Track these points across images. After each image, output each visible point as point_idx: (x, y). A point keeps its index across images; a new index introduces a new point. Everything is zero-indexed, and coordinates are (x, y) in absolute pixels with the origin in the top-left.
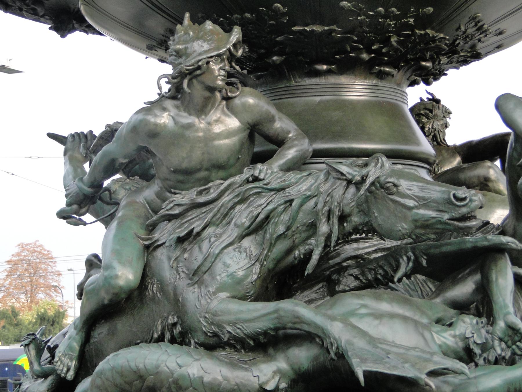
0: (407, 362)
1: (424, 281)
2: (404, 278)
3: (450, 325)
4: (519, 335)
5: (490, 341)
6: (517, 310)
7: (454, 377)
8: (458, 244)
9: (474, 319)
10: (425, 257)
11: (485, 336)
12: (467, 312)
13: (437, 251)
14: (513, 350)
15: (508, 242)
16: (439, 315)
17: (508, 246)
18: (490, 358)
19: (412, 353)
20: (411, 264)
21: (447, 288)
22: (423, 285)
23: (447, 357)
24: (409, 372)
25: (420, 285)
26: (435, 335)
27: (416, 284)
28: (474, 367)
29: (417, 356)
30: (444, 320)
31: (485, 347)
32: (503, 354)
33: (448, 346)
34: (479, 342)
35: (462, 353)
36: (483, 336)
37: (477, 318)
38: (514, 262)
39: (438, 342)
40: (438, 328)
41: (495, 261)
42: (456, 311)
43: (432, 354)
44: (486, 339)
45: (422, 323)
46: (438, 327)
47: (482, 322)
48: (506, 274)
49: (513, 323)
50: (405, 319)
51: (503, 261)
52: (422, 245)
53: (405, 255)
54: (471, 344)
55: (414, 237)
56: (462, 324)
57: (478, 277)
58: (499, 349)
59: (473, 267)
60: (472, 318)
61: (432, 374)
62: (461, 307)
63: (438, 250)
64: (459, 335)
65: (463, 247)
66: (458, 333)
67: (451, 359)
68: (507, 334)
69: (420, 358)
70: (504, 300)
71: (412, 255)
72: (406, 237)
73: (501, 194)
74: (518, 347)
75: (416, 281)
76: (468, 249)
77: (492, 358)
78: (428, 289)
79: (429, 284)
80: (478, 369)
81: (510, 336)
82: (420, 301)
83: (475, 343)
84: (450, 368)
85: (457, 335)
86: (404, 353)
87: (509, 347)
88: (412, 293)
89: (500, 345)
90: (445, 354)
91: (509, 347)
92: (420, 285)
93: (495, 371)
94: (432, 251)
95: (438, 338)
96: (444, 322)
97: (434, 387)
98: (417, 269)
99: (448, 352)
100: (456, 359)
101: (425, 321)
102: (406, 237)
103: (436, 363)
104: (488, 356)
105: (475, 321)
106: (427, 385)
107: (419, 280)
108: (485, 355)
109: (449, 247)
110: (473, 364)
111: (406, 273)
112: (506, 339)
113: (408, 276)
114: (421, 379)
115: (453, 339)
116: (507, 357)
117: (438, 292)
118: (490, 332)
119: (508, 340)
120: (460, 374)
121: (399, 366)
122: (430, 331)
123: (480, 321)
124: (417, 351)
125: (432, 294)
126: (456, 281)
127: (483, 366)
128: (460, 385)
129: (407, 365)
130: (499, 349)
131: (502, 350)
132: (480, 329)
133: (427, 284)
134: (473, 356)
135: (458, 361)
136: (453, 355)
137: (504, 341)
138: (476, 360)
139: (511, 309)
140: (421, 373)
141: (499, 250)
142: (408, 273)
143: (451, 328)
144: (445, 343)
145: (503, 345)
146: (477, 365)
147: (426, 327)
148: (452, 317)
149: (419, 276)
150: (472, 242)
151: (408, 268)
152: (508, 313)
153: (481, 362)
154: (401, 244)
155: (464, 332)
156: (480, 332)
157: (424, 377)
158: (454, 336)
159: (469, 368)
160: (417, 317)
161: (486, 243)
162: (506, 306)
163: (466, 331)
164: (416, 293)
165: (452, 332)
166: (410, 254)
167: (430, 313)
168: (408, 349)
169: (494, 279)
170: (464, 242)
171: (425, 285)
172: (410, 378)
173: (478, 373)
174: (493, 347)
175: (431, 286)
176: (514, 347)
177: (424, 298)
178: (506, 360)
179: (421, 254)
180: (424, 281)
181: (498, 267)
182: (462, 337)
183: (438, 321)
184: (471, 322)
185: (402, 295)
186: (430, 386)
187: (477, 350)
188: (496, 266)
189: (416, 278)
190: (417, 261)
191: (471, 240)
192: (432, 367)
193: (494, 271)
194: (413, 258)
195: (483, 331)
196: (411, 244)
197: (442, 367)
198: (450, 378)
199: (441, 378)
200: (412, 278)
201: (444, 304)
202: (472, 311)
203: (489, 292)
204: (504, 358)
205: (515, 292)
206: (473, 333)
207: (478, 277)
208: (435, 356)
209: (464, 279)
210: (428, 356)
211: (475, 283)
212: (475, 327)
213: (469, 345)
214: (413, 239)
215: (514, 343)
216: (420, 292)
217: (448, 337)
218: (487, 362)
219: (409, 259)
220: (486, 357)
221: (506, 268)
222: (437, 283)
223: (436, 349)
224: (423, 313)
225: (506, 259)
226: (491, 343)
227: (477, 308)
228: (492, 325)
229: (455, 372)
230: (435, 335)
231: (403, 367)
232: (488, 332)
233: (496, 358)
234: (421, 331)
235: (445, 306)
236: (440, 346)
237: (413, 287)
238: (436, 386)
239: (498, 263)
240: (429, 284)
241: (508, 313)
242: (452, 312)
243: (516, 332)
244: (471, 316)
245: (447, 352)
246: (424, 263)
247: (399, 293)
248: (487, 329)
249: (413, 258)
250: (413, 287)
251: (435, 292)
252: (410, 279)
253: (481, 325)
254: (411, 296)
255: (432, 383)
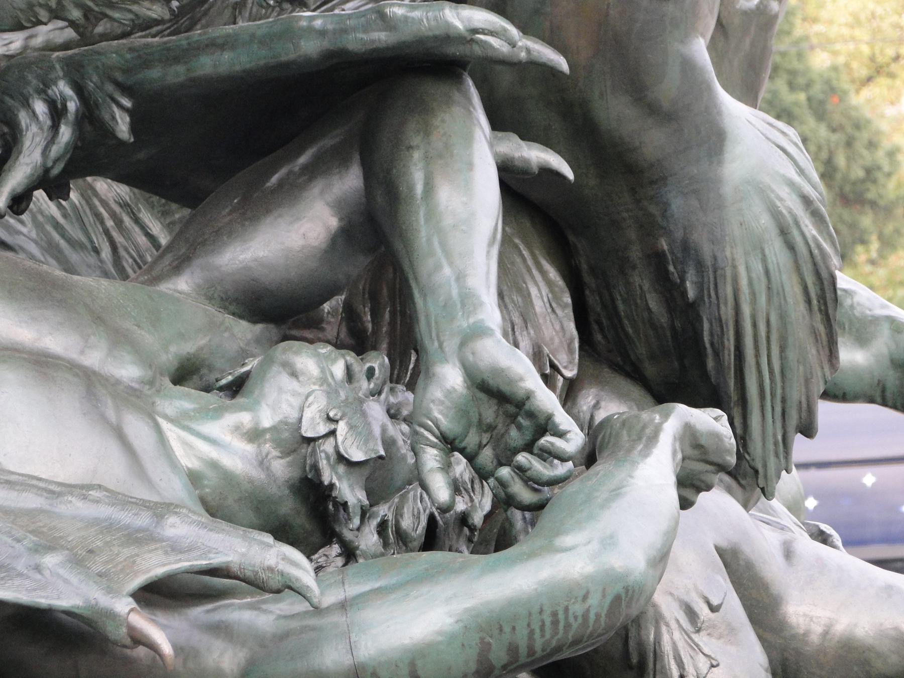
0: (50, 547)
1: (124, 205)
2: (40, 195)
3: (236, 388)
4: (523, 421)
5: (404, 449)
6: (517, 319)
7: (252, 607)
8: (266, 41)
9: (334, 361)
10: (127, 103)
11: (384, 430)
12: (308, 334)
13: (176, 74)
14: (502, 483)
15: (475, 31)
16: (189, 348)
17: (477, 50)
18: (406, 523)
19: (76, 507)
20: (66, 133)
21: (218, 232)
22: (119, 223)
23: (223, 525)
24: (59, 588)
25: (110, 223)
26: (172, 432)
27: (89, 218)
28: (340, 561)
29: (96, 522)
30: (211, 368)
31: (383, 476)
32: (461, 506)
33: (228, 477)
34: (357, 456)
35: (288, 507)
36: (377, 431)
37: (351, 357)
38: (499, 121)
39: (188, 462)
40: (180, 401)
41: (423, 109)
42: (259, 327)
43: (162, 509)
44: (389, 443)
45: (118, 382)
46: (183, 400)
47: (370, 373)
48: (470, 166)
49: (498, 372)
50: (41, 364)
51: (457, 110)
52: (113, 52)
53: (42, 92)
54: (323, 464)
55: (76, 14)
56: (285, 380)
57: (350, 181)
58: (440, 481)
59: (327, 142)
60: (327, 357)
61: (159, 594)
62: (282, 311)
63: (181, 69)
64: (274, 429)
65: (288, 53)
66: (267, 420)
67: (241, 530)
68: (475, 420)
69: (107, 527)
70: (460, 277)
71: (68, 91)
72: (43, 15)
73: (677, 523)
74: (521, 470)
75: (92, 207)
76: (308, 61)
77: (413, 523)
78: (142, 240)
79: (146, 217)
80: (352, 568)
81: (491, 428)
82: (106, 289)
83: (341, 458)
84: (235, 569)
85: (265, 431)
86: (41, 511)
87: (483, 475)
88: (74, 257)
89: (447, 467)
90: (215, 510)
91: (483, 475)
92: (110, 223)
93: (427, 577)
94: (155, 73)
95: (185, 443)
96: (212, 377)
97: (167, 648)
98: (91, 154)
99: (230, 501)
100: (263, 528)
101: (128, 371)
102: (43, 15)
103: (175, 548)
104: (398, 514)
105: (338, 370)
106: (138, 639)
107: (105, 203)
108: (384, 510)
109: (227, 56)
110: (335, 549)
111: (47, 171)
112: (471, 440)
113: (54, 184)
114: (111, 615)
115: (249, 448)
116: (477, 519)
117: (182, 253)
118: (405, 412)
119: (481, 446)
120: (278, 591)
121: (20, 565)
122: (151, 415)
123: (360, 369)
124: (97, 501)
125: (161, 257)
126: (256, 205)
127: (375, 556)
128: (282, 637)
129: (51, 560)
130: (440, 481)
131: (456, 488)
132: (361, 402)
133: (137, 221)
134: (336, 520)
135: (269, 539)
136: (251, 516)
137: (462, 451)
138: (348, 535)
139: (491, 314)
140: (110, 591)
141: (433, 65)
142: (56, 171)
143: (240, 400)
144: (214, 465)
145: (461, 467)
146: (350, 554)
147: (133, 398)
148: (243, 355)
149: (103, 186)
150: (322, 33)
151: (55, 151)
152: (479, 331)
153: (369, 540)
154: (25, 48)
155: (293, 415)
156: (364, 414)
157: (123, 605)
158: (255, 435)
159: (318, 569)
160: (94, 358)
161: (381, 37)
162: (468, 300)
163: (302, 410)
164: (92, 259)
165: (245, 418)
166: (63, 88)
167: (148, 338)
168: (57, 491)
169: (419, 189)
170: (289, 33)
171: (127, 221)
172: (68, 613)
173: (353, 589)
174: (418, 479)
175: (156, 228)
176: (505, 472)
177: (124, 276)
178: (472, 529)
179: (110, 88)
180: (124, 205)
181: (435, 137)
182: (286, 435)
183: (185, 374)
184: (323, 371)
185: (29, 263)
186: (152, 647)
187: (351, 493)
188: (427, 134)
189: (89, 194)
190: (90, 119)
191: (318, 23)
192: (156, 566)
193: (417, 155)
194: (72, 106)
195: (376, 411)
196: (66, 46)
197: (203, 563)
198: (239, 612)
199: (199, 612)
200: (74, 196)
201: (210, 298)
202: (331, 331)
203: (399, 246)
204: (464, 519)
205: (506, 241)
206: (330, 419)
207: (350, 181)
208: (172, 520)
209: (290, 192)
210: (143, 520)
211: (338, 206)
212: (343, 395)
213: (316, 468)
214: (73, 24)
215: (505, 458)
216: (106, 253)
217: (227, 438)
218: (394, 537)
219: (57, 112)
220: (390, 517)
221: (468, 139)
222: (181, 213)
223: (175, 488)
224: (120, 339)
225: (469, 113)
226: (411, 460)
227: (350, 314)
228: (411, 386)
229: (258, 585)
230: (172, 432)
231: (38, 568)
232: (393, 414)
233: (432, 519)
234: (111, 414)
235: (211, 309)
236: (194, 478)
237: (76, 233)
238: (178, 649)
239: (436, 122)
240: (146, 217)
241: (479, 331)
242: (245, 331)
243: (511, 409)
244: (325, 349)
245: (222, 502)
246: (123, 126)
247: (22, 256)
248: (392, 400)
249: (72, 106)
250: (76, 233)
251: (170, 247)
252: (66, 197)
253: (365, 385)
254: (70, 269)
255: (160, 632)
